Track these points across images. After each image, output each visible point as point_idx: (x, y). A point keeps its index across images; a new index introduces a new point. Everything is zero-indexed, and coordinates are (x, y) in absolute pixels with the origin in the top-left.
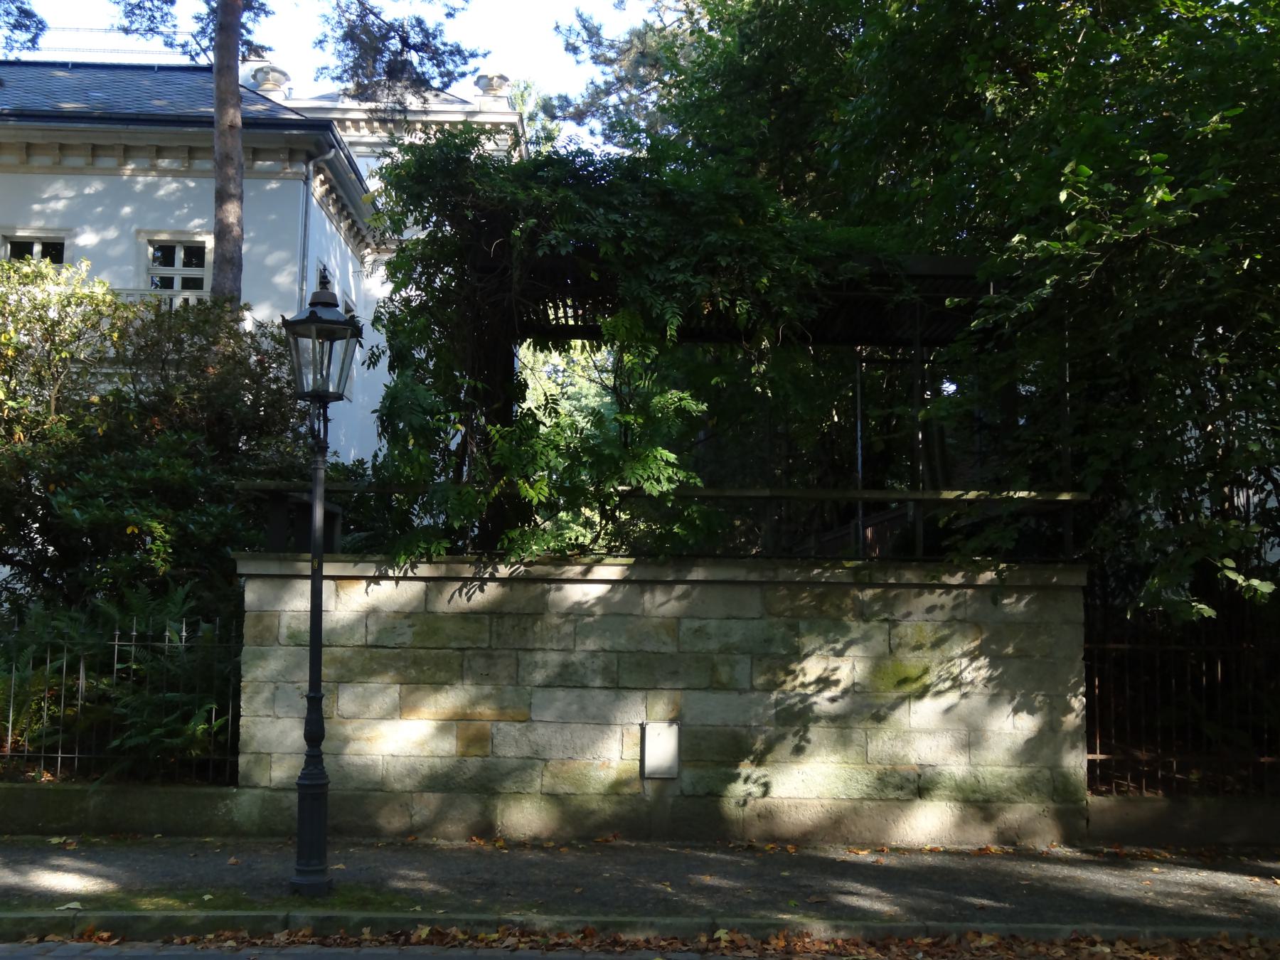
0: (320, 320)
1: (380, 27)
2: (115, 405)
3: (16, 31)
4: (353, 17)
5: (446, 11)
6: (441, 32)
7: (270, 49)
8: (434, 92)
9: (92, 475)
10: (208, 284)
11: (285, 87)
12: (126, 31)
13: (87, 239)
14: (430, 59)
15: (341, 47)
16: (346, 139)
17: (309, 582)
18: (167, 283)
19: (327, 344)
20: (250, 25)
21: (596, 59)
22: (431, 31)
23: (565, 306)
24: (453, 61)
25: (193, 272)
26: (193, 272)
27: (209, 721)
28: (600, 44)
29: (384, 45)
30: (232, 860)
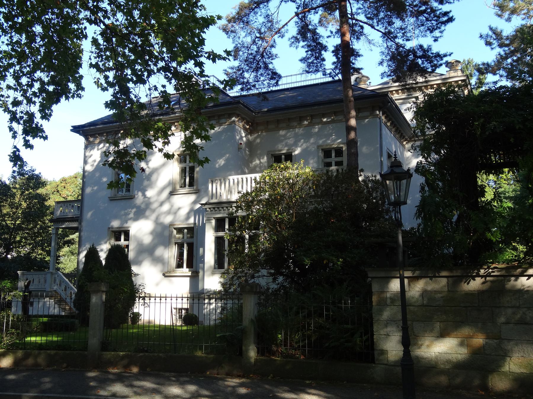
0: (395, 173)
1: (405, 52)
2: (315, 213)
3: (271, 81)
4: (394, 50)
5: (433, 39)
6: (431, 49)
7: (362, 69)
8: (429, 74)
9: (309, 241)
10: (345, 163)
11: (369, 81)
12: (308, 72)
13: (297, 151)
14: (426, 61)
15: (390, 63)
16: (394, 98)
17: (399, 279)
18: (329, 165)
19: (398, 182)
20: (353, 61)
21: (501, 46)
22: (426, 49)
23: (500, 155)
24: (437, 60)
25: (339, 159)
26: (339, 159)
27: (361, 337)
28: (502, 39)
29: (407, 59)
30: (376, 394)
